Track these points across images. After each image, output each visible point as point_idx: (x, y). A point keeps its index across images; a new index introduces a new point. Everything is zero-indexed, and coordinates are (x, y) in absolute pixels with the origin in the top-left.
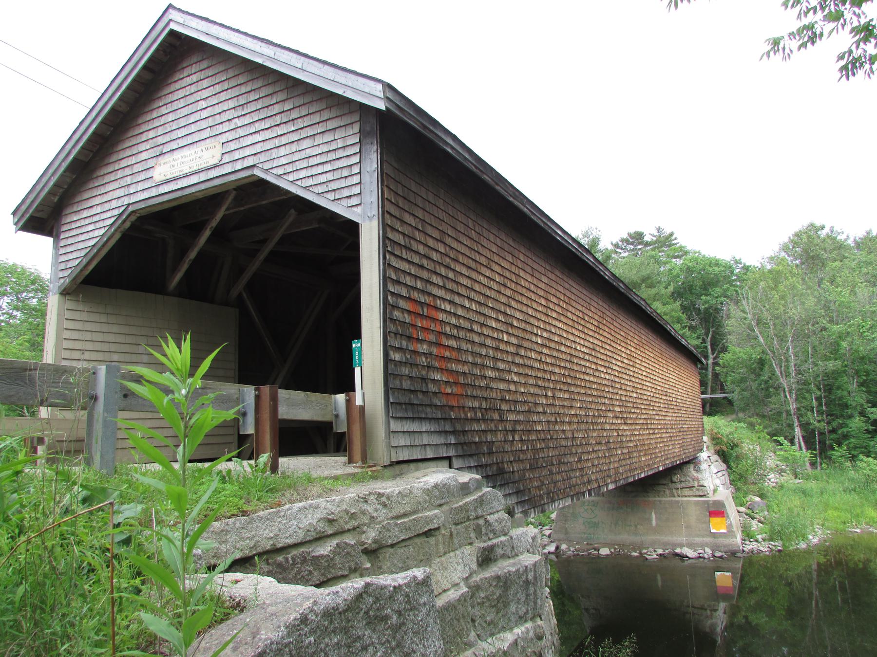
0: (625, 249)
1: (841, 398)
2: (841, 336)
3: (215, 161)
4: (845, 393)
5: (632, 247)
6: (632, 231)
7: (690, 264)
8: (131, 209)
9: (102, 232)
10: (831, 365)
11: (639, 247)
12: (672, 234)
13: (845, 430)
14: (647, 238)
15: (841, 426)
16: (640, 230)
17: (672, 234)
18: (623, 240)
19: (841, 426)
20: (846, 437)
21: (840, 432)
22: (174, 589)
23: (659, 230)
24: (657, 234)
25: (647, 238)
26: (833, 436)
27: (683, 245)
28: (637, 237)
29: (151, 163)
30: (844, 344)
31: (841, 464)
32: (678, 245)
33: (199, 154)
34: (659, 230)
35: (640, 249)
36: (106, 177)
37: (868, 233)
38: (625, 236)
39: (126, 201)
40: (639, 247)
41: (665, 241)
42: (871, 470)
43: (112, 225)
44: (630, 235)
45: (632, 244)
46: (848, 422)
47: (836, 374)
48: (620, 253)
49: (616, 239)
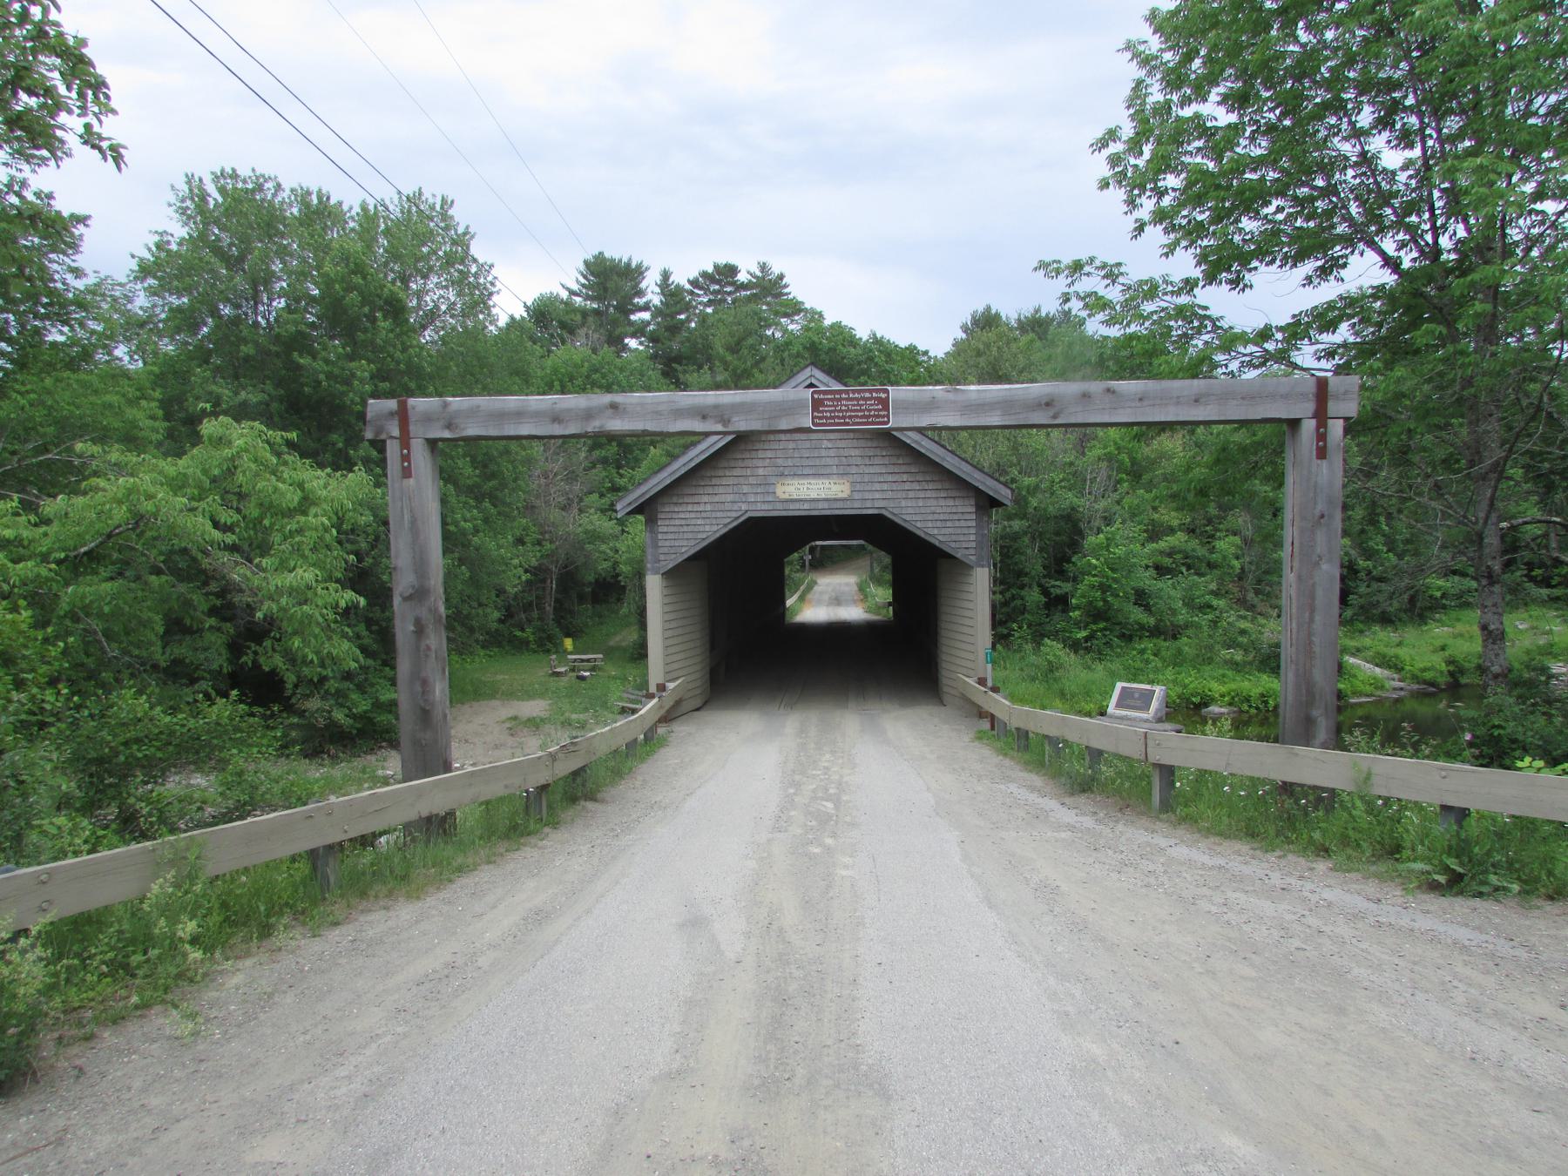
0: (707, 291)
1: (1016, 563)
2: (1033, 490)
3: (844, 495)
4: (1023, 558)
5: (717, 287)
6: (722, 261)
7: (815, 339)
8: (749, 515)
9: (715, 528)
10: (1017, 525)
11: (728, 289)
12: (781, 277)
13: (1018, 602)
14: (742, 277)
15: (1013, 598)
16: (732, 261)
17: (781, 277)
18: (704, 275)
19: (1013, 598)
20: (1023, 610)
21: (1012, 605)
22: (1358, 725)
23: (763, 267)
24: (759, 274)
25: (742, 277)
26: (1005, 610)
27: (800, 299)
28: (727, 272)
29: (773, 480)
30: (1034, 502)
31: (1020, 646)
32: (791, 297)
33: (827, 486)
34: (763, 267)
35: (729, 293)
37: (1037, 311)
38: (710, 270)
39: (744, 507)
40: (728, 289)
41: (769, 287)
42: (1055, 655)
43: (725, 525)
44: (716, 267)
45: (718, 282)
46: (1023, 593)
47: (1015, 537)
48: (699, 296)
49: (694, 274)
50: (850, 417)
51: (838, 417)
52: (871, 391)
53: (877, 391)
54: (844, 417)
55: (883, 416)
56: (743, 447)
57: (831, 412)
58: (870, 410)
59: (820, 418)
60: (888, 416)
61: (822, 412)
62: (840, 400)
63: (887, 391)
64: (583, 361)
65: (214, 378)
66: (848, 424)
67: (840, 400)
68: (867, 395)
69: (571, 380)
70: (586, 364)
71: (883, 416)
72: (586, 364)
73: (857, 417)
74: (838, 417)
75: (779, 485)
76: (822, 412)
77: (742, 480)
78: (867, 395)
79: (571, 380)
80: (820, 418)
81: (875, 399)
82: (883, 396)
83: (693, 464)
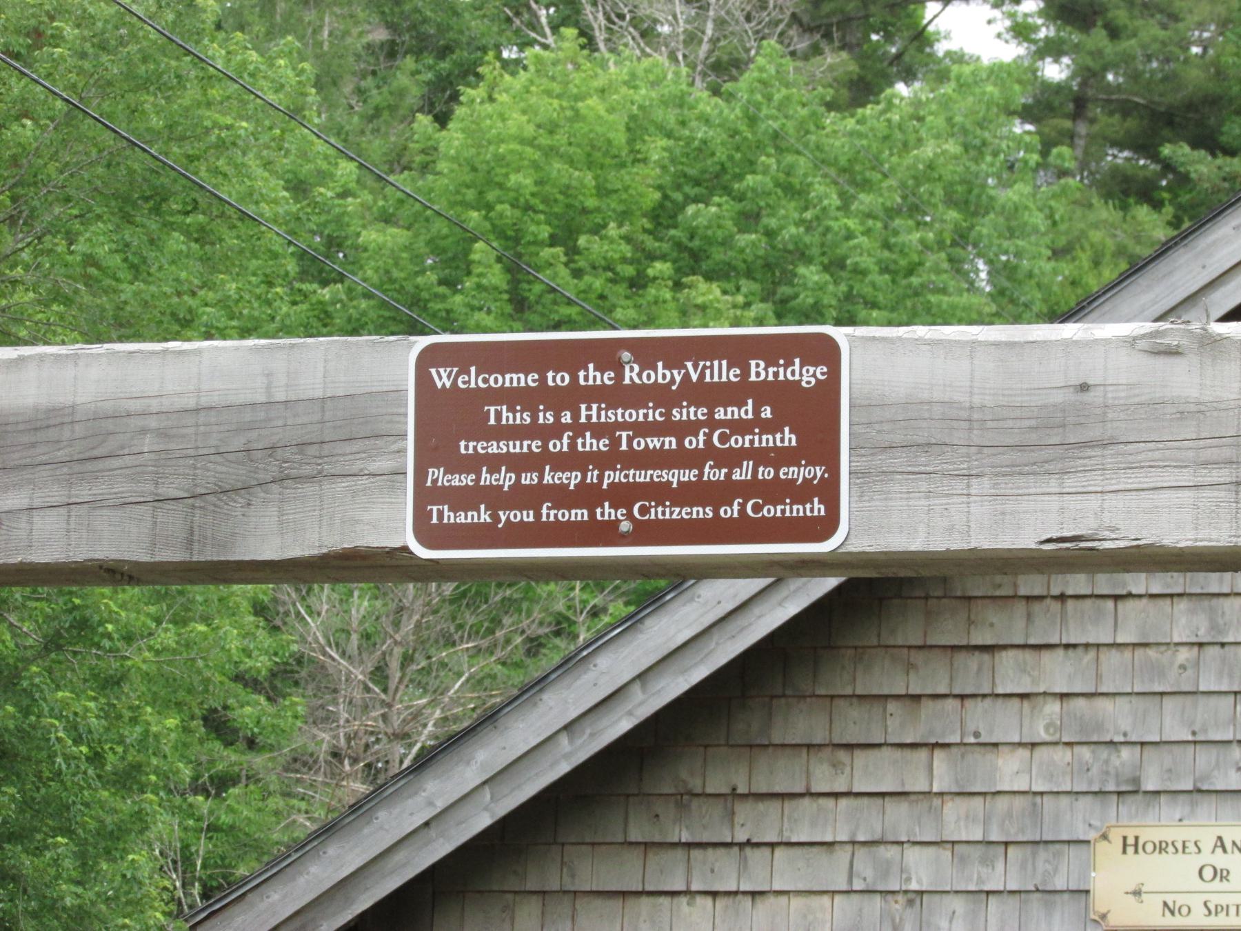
36: (744, 811)
50: (623, 496)
51: (561, 497)
52: (738, 351)
53: (773, 349)
54: (588, 496)
55: (802, 493)
56: (910, 633)
57: (518, 463)
58: (731, 459)
59: (463, 499)
60: (829, 491)
61: (473, 464)
62: (573, 396)
63: (826, 352)
64: (637, 127)
65: (295, 173)
66: (606, 533)
67: (573, 396)
68: (721, 372)
69: (565, 237)
70: (656, 148)
71: (802, 493)
72: (656, 148)
73: (660, 493)
74: (561, 497)
75: (1108, 853)
76: (473, 464)
77: (899, 819)
78: (721, 372)
79: (565, 237)
80: (463, 499)
81: (763, 393)
82: (808, 375)
83: (619, 725)
